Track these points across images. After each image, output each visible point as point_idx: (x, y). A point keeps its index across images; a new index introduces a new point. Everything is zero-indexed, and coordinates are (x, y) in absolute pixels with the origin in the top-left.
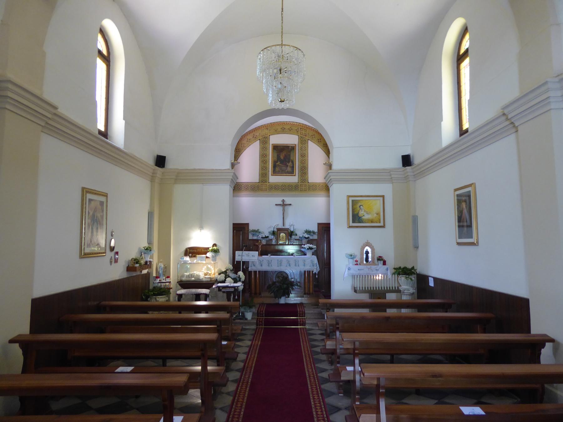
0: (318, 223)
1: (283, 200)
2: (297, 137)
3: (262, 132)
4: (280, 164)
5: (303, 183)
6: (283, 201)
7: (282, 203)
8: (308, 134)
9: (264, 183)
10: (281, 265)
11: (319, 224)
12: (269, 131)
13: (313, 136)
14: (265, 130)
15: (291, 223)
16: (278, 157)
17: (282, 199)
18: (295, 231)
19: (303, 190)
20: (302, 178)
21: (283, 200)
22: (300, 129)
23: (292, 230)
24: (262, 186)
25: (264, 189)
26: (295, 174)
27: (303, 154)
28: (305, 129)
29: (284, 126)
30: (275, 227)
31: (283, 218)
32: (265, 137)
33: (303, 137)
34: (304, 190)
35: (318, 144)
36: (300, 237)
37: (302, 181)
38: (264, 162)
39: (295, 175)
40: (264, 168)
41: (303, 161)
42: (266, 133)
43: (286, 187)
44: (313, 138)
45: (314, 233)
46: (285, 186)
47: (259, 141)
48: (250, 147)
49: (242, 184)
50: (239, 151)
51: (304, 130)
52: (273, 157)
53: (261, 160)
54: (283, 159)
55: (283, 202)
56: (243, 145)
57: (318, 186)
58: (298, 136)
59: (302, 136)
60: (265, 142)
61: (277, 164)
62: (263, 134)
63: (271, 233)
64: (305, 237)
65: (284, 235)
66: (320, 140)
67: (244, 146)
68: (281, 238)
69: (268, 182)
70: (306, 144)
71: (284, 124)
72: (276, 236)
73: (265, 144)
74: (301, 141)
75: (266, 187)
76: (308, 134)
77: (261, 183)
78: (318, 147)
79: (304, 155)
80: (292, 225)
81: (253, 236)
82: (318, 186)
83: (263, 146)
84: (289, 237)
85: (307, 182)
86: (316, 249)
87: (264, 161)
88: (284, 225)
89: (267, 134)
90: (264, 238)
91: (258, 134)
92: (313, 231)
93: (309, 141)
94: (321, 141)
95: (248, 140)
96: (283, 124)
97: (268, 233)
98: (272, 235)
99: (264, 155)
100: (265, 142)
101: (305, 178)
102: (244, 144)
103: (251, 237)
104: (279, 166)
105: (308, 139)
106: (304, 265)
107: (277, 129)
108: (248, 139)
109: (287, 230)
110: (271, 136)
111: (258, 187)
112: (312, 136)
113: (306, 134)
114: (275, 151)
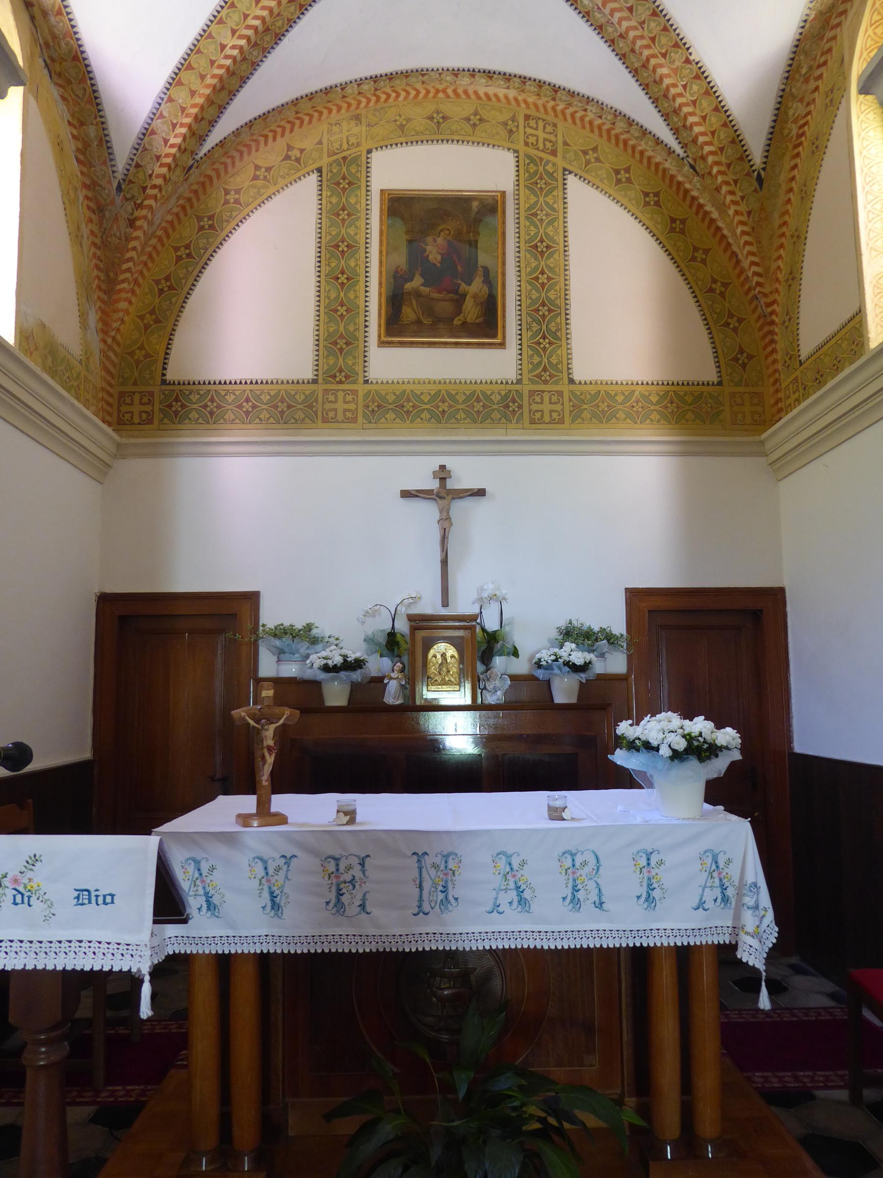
0: (627, 590)
1: (443, 467)
2: (510, 157)
3: (329, 131)
4: (425, 290)
5: (546, 382)
6: (443, 474)
7: (434, 485)
8: (565, 144)
9: (340, 382)
10: (445, 903)
11: (634, 596)
12: (364, 128)
13: (591, 156)
14: (344, 124)
15: (490, 589)
16: (417, 258)
17: (434, 462)
18: (507, 629)
19: (547, 418)
20: (536, 359)
21: (443, 467)
22: (521, 120)
23: (491, 623)
24: (332, 398)
25: (340, 417)
26: (504, 337)
27: (542, 241)
28: (550, 118)
29: (442, 107)
30: (402, 610)
31: (444, 562)
32: (344, 158)
33: (541, 159)
34: (552, 421)
35: (614, 194)
36: (538, 664)
37: (539, 376)
38: (343, 279)
39: (502, 345)
40: (342, 310)
41: (543, 273)
42: (353, 140)
43: (457, 402)
44: (588, 162)
45: (611, 639)
46: (452, 397)
47: (314, 177)
48: (269, 205)
49: (228, 392)
50: (212, 227)
51: (546, 124)
52: (386, 250)
53: (325, 269)
54: (442, 262)
55: (443, 480)
56: (231, 197)
57: (620, 398)
58: (515, 151)
59: (532, 152)
60: (344, 184)
61: (408, 286)
62: (337, 145)
63: (379, 644)
64: (567, 664)
65: (451, 651)
66: (623, 176)
67: (237, 202)
68: (432, 670)
69: (361, 380)
70: (555, 193)
71: (441, 95)
72: (405, 659)
73: (344, 190)
74: (532, 176)
75: (352, 406)
76: (565, 144)
77: (326, 382)
78: (616, 208)
79: (548, 247)
80: (493, 597)
81: (279, 661)
82: (620, 398)
83: (334, 200)
84: (480, 667)
85: (566, 380)
86: (737, 756)
87: (343, 273)
88: (445, 604)
89: (358, 145)
90: (335, 669)
91: (308, 144)
92: (602, 630)
93: (571, 180)
94: (629, 180)
95: (261, 173)
96: (435, 97)
97: (364, 646)
98: (381, 656)
99: (343, 247)
100: (344, 184)
101: (554, 360)
102: (238, 192)
103: (268, 666)
104: (418, 294)
105: (565, 170)
106: (650, 900)
107: (408, 120)
108: (257, 168)
109: (470, 621)
110: (374, 155)
111: (310, 404)
112: (585, 153)
113: (554, 144)
114: (399, 223)
